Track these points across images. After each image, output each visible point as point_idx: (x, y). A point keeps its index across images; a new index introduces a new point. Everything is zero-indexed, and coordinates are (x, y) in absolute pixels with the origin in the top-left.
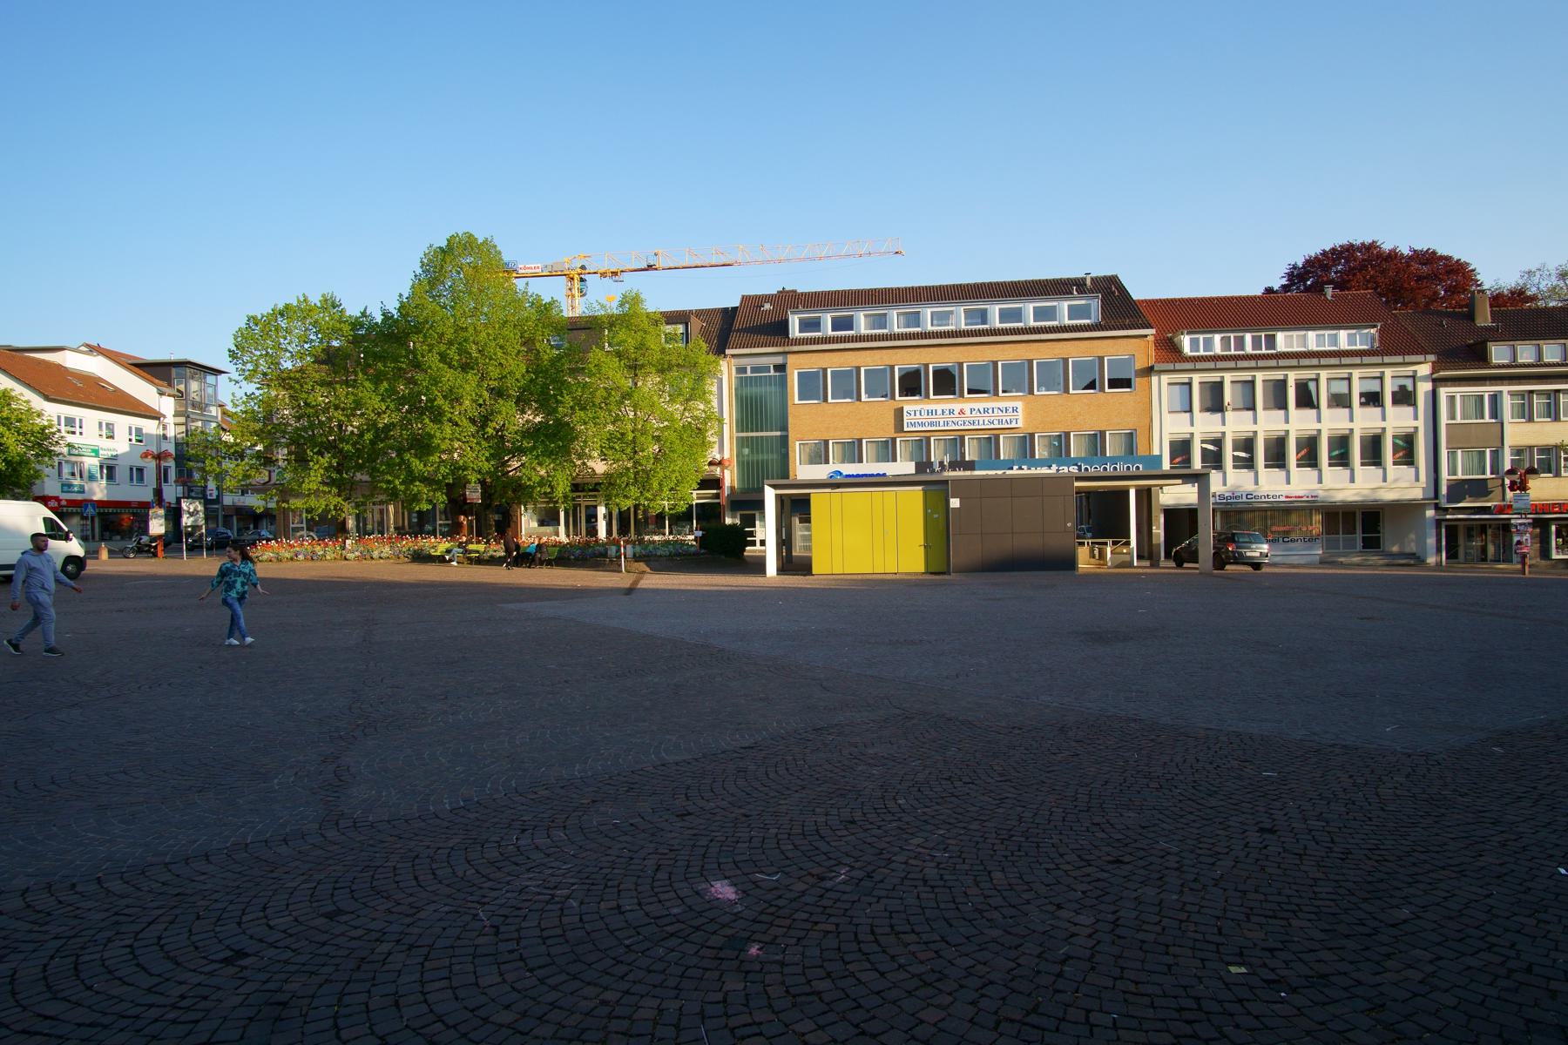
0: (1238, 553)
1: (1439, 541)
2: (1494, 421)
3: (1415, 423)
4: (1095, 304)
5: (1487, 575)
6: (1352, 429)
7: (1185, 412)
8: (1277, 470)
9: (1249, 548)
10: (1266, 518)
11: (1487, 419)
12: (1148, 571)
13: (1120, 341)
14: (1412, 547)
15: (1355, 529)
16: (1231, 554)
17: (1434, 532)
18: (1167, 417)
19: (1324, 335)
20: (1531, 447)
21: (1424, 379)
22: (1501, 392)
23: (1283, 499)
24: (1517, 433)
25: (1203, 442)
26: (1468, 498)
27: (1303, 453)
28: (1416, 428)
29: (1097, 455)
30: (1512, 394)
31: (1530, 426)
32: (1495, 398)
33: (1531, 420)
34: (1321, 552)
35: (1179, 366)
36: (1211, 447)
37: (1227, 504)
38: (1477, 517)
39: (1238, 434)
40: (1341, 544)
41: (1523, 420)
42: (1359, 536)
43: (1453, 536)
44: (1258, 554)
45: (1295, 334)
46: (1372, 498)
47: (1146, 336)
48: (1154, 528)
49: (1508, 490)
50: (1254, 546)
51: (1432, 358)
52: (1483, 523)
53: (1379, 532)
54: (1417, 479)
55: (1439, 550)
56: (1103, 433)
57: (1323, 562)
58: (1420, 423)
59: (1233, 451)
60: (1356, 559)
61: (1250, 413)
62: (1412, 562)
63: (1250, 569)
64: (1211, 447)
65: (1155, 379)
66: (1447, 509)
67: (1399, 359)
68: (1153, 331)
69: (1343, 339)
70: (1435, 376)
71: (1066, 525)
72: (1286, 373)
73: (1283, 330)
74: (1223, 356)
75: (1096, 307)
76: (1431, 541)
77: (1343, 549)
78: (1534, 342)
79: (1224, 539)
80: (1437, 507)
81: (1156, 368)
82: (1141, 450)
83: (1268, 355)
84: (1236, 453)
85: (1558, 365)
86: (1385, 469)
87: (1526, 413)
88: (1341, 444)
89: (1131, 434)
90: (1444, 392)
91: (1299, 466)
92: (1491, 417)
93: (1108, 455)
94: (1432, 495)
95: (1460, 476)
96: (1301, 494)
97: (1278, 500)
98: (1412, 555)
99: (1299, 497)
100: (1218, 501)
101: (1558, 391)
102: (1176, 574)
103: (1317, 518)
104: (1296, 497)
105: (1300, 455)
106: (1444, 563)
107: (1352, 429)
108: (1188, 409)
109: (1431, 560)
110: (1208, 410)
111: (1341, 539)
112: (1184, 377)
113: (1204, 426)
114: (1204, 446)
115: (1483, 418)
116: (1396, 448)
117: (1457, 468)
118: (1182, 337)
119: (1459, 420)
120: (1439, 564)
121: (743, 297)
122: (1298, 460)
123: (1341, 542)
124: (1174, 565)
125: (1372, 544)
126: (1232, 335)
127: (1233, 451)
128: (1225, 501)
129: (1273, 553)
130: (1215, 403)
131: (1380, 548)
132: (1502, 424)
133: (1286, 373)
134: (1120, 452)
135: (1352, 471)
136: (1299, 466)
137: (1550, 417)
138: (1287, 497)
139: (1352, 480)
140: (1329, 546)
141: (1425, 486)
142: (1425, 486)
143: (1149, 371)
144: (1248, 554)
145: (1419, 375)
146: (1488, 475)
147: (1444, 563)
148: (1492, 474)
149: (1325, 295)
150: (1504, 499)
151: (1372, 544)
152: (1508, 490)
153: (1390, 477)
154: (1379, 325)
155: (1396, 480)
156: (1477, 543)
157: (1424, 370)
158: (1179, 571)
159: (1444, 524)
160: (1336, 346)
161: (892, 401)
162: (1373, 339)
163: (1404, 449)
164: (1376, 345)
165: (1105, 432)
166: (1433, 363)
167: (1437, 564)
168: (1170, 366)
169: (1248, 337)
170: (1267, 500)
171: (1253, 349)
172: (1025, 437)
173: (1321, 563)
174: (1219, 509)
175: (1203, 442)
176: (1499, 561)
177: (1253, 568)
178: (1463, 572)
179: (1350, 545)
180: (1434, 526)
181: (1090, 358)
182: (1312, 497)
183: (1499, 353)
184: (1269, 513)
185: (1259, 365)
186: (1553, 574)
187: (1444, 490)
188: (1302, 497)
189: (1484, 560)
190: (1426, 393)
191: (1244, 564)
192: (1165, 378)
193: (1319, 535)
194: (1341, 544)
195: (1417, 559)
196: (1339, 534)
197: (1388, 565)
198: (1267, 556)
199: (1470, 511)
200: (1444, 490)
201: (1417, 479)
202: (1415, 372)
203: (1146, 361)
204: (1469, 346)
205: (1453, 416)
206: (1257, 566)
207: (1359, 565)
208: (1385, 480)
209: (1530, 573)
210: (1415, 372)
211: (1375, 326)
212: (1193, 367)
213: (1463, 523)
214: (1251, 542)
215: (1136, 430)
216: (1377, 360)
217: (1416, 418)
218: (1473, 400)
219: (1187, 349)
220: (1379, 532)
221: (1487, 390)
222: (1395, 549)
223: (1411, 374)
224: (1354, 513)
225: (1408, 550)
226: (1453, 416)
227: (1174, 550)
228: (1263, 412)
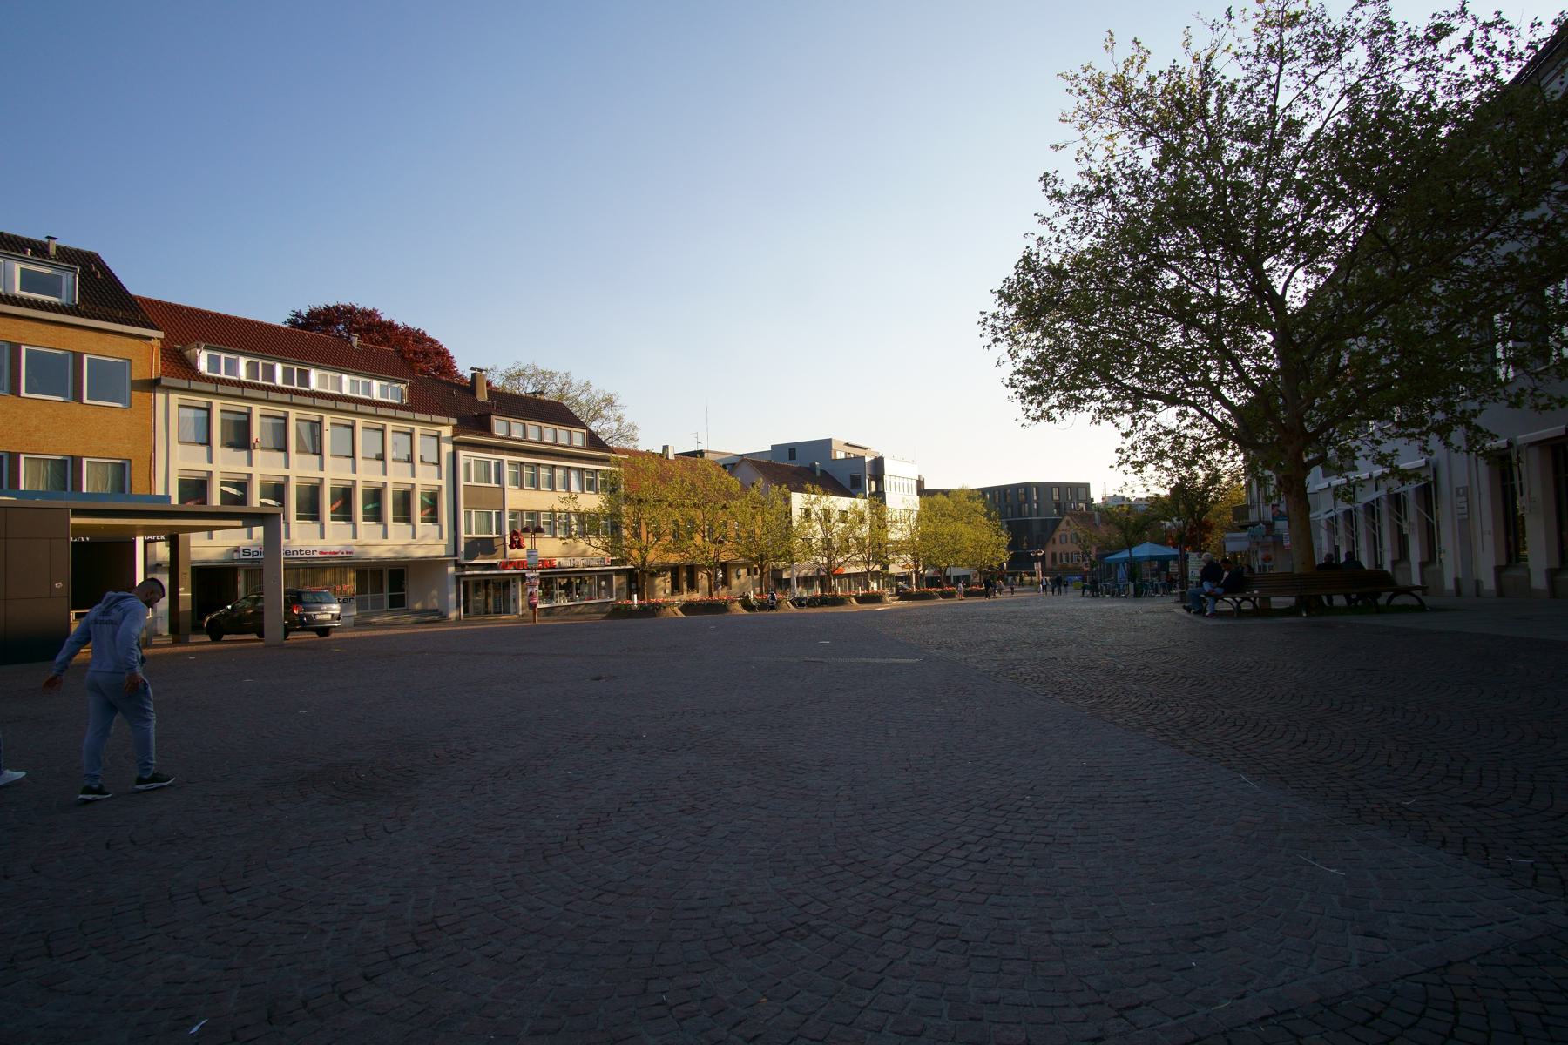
0: (307, 616)
1: (458, 596)
2: (497, 486)
3: (438, 482)
4: (70, 281)
5: (499, 626)
6: (323, 479)
7: (202, 444)
8: (310, 522)
9: (319, 610)
10: (298, 575)
11: (493, 484)
12: (210, 647)
13: (110, 337)
14: (435, 604)
15: (381, 587)
16: (297, 619)
17: (453, 587)
18: (176, 449)
19: (358, 381)
20: (522, 511)
21: (447, 440)
22: (502, 460)
23: (317, 555)
24: (517, 499)
25: (223, 483)
26: (480, 556)
27: (337, 505)
28: (440, 487)
29: (66, 489)
30: (511, 463)
31: (521, 492)
32: (499, 464)
33: (522, 488)
34: (355, 613)
35: (195, 385)
36: (233, 491)
37: (253, 560)
38: (488, 572)
39: (187, 473)
40: (369, 605)
41: (517, 487)
42: (386, 594)
43: (470, 586)
44: (329, 617)
45: (330, 374)
46: (402, 555)
47: (150, 338)
48: (181, 589)
49: (508, 548)
50: (325, 607)
51: (453, 421)
52: (486, 578)
53: (403, 590)
54: (441, 537)
55: (458, 606)
56: (77, 461)
57: (358, 625)
58: (443, 483)
59: (261, 498)
60: (389, 619)
61: (281, 455)
62: (436, 618)
63: (315, 635)
64: (233, 491)
65: (160, 397)
66: (464, 565)
67: (427, 418)
68: (161, 334)
69: (377, 389)
70: (455, 439)
71: (51, 586)
72: (210, 400)
73: (318, 367)
74: (283, 388)
75: (70, 282)
76: (452, 596)
77: (372, 608)
78: (566, 428)
79: (295, 598)
80: (457, 564)
81: (163, 383)
82: (138, 488)
83: (264, 385)
84: (264, 501)
85: (565, 446)
86: (414, 526)
87: (518, 482)
88: (344, 497)
89: (123, 465)
90: (463, 455)
91: (333, 519)
92: (496, 483)
93: (85, 490)
94: (453, 553)
95: (474, 535)
96: (335, 549)
97: (311, 556)
98: (435, 612)
99: (334, 553)
100: (242, 557)
101: (538, 465)
102: (209, 651)
103: (352, 575)
104: (330, 553)
105: (334, 507)
106: (462, 617)
107: (386, 483)
108: (205, 441)
109: (452, 615)
110: (230, 445)
111: (369, 599)
112: (202, 400)
113: (224, 464)
114: (225, 488)
115: (490, 483)
116: (424, 506)
117: (471, 528)
118: (198, 351)
119: (473, 483)
120: (458, 618)
121: (1088, 484)
122: (332, 512)
123: (369, 602)
124: (207, 638)
125: (397, 602)
126: (260, 362)
127: (261, 498)
128: (251, 557)
129: (345, 614)
130: (240, 438)
131: (404, 606)
132: (504, 489)
133: (322, 414)
134: (105, 487)
135: (385, 526)
136: (333, 519)
137: (533, 486)
138: (321, 553)
139: (385, 536)
140: (361, 606)
141: (447, 543)
142: (447, 543)
143: (153, 385)
144: (318, 617)
145: (443, 436)
146: (494, 535)
147: (462, 617)
148: (496, 533)
149: (351, 343)
150: (505, 557)
151: (397, 602)
152: (508, 548)
153: (419, 534)
154: (409, 381)
155: (424, 537)
156: (480, 598)
157: (447, 432)
158: (179, 649)
159: (462, 580)
160: (369, 395)
161: (14, 398)
162: (402, 394)
163: (430, 506)
164: (405, 401)
165: (80, 459)
166: (454, 426)
167: (456, 617)
168: (185, 384)
169: (279, 368)
170: (299, 556)
171: (284, 383)
172: (64, 462)
173: (355, 625)
174: (242, 566)
175: (223, 483)
176: (500, 613)
177: (318, 634)
178: (478, 626)
179: (377, 604)
180: (454, 582)
181: (60, 352)
182: (347, 553)
183: (499, 425)
184: (301, 571)
185: (317, 404)
186: (568, 620)
187: (462, 548)
188: (336, 553)
189: (487, 613)
190: (448, 453)
191: (312, 630)
192: (175, 398)
193: (353, 595)
194: (369, 605)
195: (440, 615)
196: (367, 593)
197: (417, 623)
198: (339, 619)
199: (482, 568)
200: (462, 548)
201: (441, 537)
202: (439, 432)
203: (148, 370)
204: (475, 416)
205: (468, 479)
206: (324, 631)
207: (391, 625)
208: (414, 537)
209: (539, 621)
210: (439, 432)
211: (404, 382)
212: (214, 390)
213: (472, 579)
214: (321, 603)
215: (130, 460)
216: (408, 415)
217: (440, 478)
218: (483, 465)
219: (203, 366)
220: (403, 590)
221: (493, 457)
222: (418, 606)
223: (436, 434)
224: (381, 571)
225: (430, 607)
226: (468, 479)
227: (208, 619)
228: (179, 446)
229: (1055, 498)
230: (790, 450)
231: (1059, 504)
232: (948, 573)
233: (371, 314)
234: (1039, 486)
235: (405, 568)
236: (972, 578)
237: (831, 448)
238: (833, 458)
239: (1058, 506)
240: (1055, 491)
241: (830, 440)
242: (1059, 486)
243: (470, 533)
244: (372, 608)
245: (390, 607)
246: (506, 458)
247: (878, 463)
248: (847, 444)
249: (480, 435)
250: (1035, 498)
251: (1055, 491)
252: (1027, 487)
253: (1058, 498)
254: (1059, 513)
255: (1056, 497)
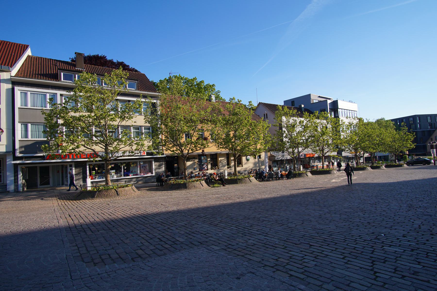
229: (429, 121)
230: (292, 102)
231: (431, 124)
232: (376, 155)
233: (98, 56)
234: (420, 116)
235: (2, 160)
236: (390, 158)
237: (310, 98)
238: (311, 103)
239: (431, 125)
240: (429, 118)
241: (309, 95)
242: (431, 116)
243: (26, 136)
244: (124, 176)
245: (365, 157)
246: (59, 92)
247: (335, 104)
248: (319, 97)
249: (51, 80)
250: (418, 121)
251: (429, 118)
252: (414, 117)
253: (430, 121)
254: (431, 128)
255: (429, 121)
